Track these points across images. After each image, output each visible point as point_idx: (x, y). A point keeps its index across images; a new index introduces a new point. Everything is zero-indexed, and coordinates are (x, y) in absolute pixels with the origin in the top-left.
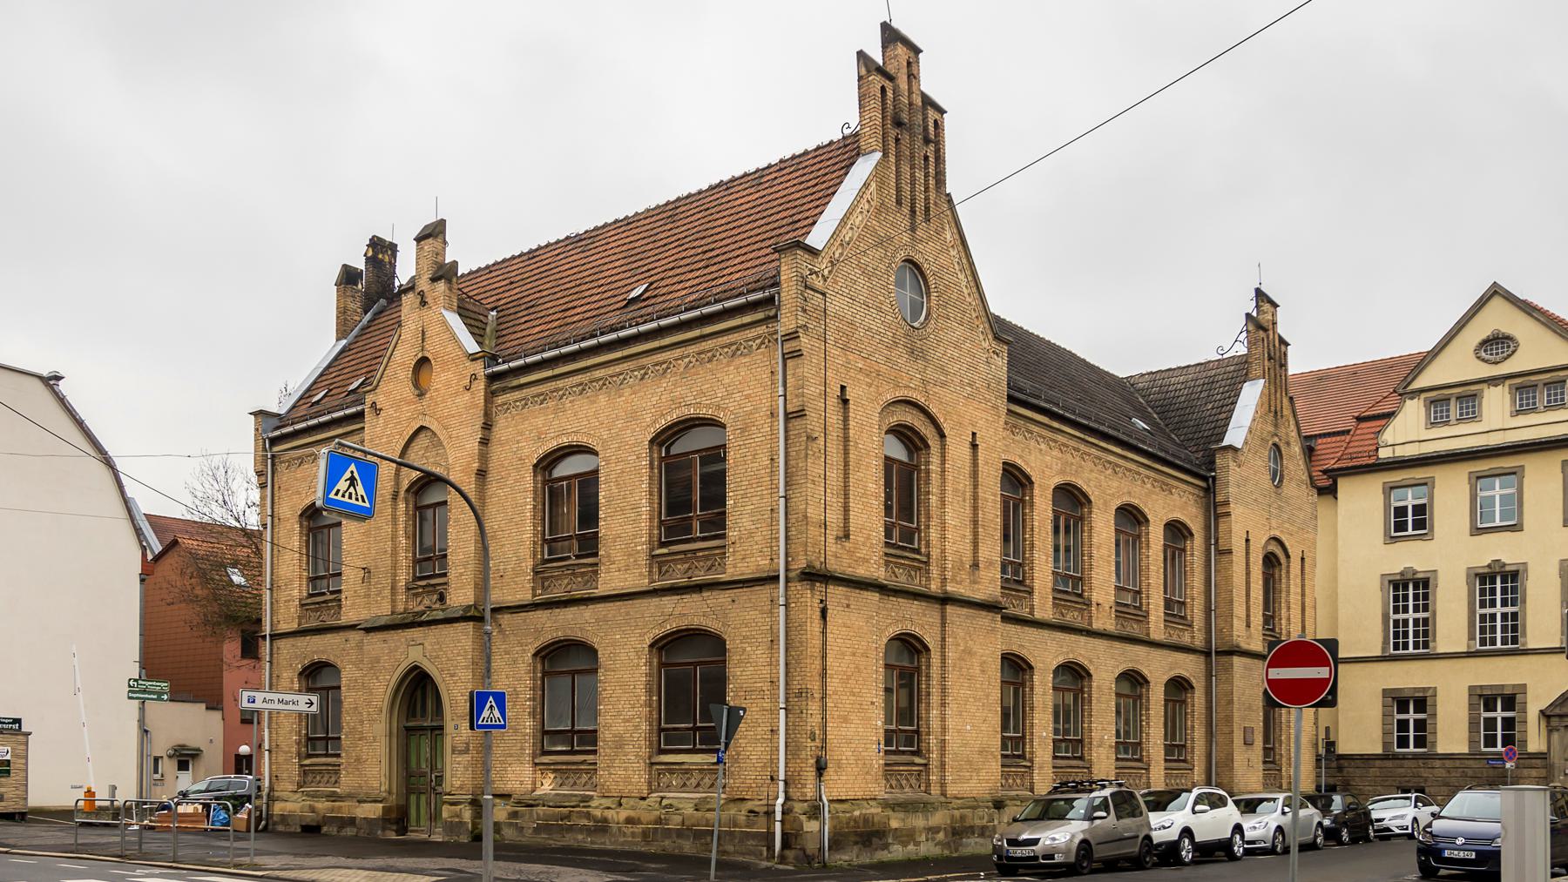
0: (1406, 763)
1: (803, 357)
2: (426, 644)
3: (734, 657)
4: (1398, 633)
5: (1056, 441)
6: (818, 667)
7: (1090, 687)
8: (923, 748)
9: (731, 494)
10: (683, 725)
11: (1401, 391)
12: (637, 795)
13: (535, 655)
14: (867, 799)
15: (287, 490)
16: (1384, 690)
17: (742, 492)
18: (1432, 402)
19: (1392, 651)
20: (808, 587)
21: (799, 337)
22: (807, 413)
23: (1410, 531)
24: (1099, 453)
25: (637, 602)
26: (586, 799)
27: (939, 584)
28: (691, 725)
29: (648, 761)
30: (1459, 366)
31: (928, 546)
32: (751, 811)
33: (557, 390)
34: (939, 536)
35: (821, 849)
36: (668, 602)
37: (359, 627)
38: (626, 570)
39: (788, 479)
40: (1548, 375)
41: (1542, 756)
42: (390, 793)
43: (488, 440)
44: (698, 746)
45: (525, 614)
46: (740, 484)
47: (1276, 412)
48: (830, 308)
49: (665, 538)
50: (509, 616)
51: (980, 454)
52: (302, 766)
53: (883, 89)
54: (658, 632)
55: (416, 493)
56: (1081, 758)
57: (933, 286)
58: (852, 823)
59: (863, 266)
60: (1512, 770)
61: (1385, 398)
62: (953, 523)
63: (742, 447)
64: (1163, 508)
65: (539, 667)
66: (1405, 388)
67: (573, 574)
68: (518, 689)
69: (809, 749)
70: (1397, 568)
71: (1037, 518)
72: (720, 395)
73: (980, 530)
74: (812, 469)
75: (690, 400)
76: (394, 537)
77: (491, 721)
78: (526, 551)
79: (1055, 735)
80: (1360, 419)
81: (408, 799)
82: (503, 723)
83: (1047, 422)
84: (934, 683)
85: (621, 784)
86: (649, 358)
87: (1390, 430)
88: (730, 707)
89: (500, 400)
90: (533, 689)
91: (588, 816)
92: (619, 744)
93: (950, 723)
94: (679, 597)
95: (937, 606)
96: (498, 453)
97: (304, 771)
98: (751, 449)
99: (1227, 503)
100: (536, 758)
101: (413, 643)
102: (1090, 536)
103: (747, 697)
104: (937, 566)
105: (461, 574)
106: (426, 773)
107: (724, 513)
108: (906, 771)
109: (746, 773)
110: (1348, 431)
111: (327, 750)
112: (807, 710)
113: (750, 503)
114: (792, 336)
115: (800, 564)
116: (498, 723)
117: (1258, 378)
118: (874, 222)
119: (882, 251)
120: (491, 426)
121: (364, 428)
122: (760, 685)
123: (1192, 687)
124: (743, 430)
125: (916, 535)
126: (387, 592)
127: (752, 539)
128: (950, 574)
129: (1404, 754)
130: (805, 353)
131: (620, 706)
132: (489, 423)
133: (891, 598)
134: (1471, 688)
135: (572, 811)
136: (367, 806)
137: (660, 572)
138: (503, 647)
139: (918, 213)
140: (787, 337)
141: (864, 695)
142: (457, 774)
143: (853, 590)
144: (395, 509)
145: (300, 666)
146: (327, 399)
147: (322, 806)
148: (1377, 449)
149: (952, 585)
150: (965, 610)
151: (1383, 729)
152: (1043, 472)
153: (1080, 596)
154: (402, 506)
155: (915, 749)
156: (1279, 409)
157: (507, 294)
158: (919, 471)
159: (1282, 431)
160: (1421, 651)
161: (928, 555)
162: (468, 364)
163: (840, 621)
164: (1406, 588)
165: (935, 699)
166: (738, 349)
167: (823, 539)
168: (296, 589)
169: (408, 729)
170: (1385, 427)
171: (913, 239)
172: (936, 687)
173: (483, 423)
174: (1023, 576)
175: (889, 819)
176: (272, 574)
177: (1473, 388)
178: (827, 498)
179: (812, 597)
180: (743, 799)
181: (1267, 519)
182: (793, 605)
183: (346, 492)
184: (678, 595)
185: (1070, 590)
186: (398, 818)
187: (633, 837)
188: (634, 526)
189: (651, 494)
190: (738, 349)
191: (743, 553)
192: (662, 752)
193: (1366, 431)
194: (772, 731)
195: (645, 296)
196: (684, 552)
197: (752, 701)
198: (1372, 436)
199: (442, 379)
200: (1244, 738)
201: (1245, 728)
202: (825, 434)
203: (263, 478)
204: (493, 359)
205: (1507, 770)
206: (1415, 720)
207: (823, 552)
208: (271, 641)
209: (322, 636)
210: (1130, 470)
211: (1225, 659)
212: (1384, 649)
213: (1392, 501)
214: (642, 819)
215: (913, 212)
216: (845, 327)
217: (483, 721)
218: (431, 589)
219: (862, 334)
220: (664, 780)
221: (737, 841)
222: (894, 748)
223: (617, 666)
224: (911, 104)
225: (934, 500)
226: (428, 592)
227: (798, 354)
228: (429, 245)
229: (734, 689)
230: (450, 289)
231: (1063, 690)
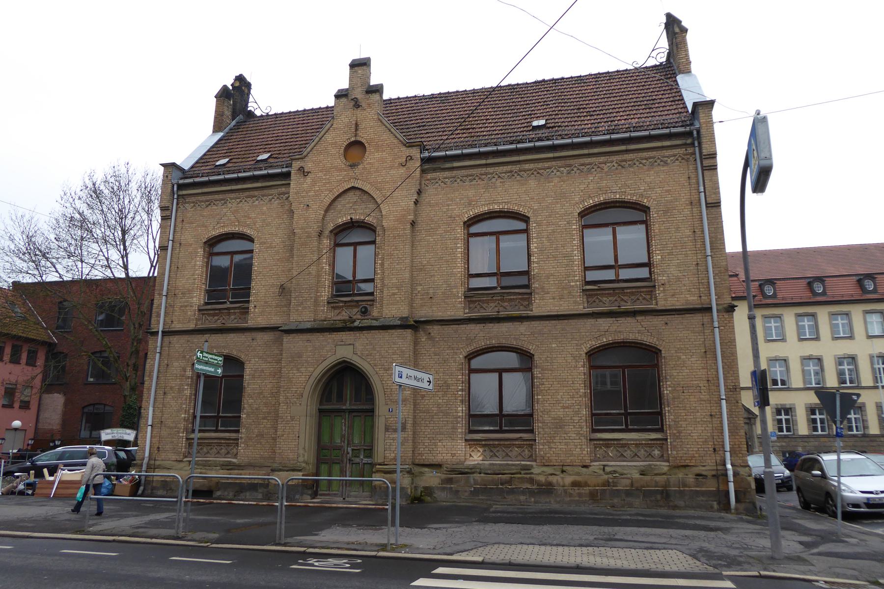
2: (357, 344)
3: (670, 363)
10: (614, 411)
12: (579, 464)
25: (573, 322)
26: (527, 468)
28: (216, 414)
33: (486, 174)
37: (280, 329)
39: (169, 287)
45: (457, 326)
46: (666, 246)
50: (440, 327)
55: (336, 235)
63: (665, 222)
67: (501, 300)
75: (615, 189)
85: (562, 455)
91: (531, 481)
92: (559, 424)
94: (614, 319)
98: (674, 224)
103: (685, 391)
105: (394, 294)
109: (689, 446)
111: (217, 426)
113: (676, 259)
122: (696, 382)
124: (666, 212)
127: (680, 283)
131: (559, 397)
135: (514, 477)
138: (433, 349)
140: (708, 157)
147: (215, 474)
162: (403, 149)
187: (580, 497)
188: (567, 268)
191: (673, 291)
194: (711, 415)
197: (690, 394)
203: (167, 213)
208: (163, 336)
209: (224, 335)
214: (589, 482)
218: (355, 304)
226: (348, 306)
229: (672, 385)
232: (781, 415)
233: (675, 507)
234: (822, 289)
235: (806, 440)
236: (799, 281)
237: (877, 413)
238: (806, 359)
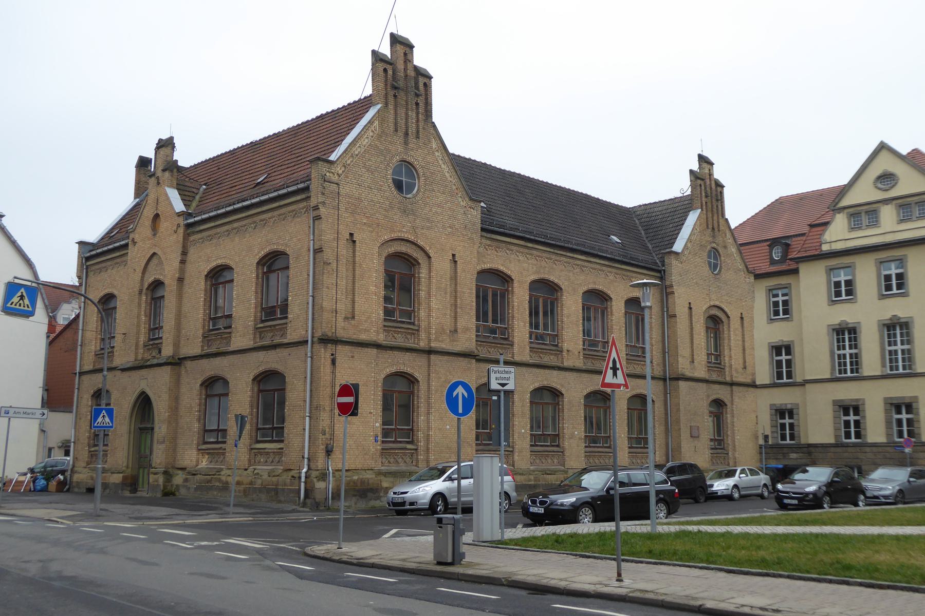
0: (850, 449)
1: (322, 219)
5: (532, 255)
6: (329, 392)
7: (563, 401)
8: (415, 440)
9: (290, 294)
11: (832, 208)
13: (201, 385)
14: (365, 470)
15: (92, 287)
17: (295, 293)
18: (851, 215)
20: (322, 346)
21: (319, 208)
22: (324, 250)
23: (844, 297)
24: (569, 260)
27: (427, 342)
29: (249, 447)
30: (864, 193)
31: (419, 320)
32: (293, 477)
34: (427, 314)
35: (326, 499)
36: (261, 355)
38: (244, 336)
42: (127, 467)
43: (185, 261)
44: (274, 438)
47: (713, 229)
48: (342, 192)
49: (265, 318)
51: (458, 266)
52: (90, 451)
53: (385, 70)
54: (257, 372)
56: (558, 446)
57: (422, 174)
58: (352, 484)
59: (368, 167)
60: (910, 454)
61: (823, 215)
62: (436, 307)
64: (624, 290)
65: (204, 392)
66: (834, 206)
67: (221, 338)
68: (193, 405)
69: (321, 440)
70: (887, 316)
71: (516, 300)
72: (287, 239)
73: (458, 310)
74: (327, 280)
76: (139, 316)
77: (103, 424)
78: (199, 324)
79: (531, 431)
81: (138, 472)
82: (111, 425)
83: (523, 244)
84: (422, 400)
86: (257, 217)
88: (242, 416)
89: (192, 238)
90: (200, 405)
91: (220, 480)
93: (433, 425)
94: (266, 352)
95: (425, 355)
96: (190, 268)
97: (91, 455)
99: (671, 286)
100: (199, 446)
101: (142, 378)
102: (562, 310)
103: (294, 410)
104: (425, 332)
106: (148, 455)
107: (287, 304)
108: (402, 453)
112: (320, 417)
114: (316, 208)
115: (318, 334)
116: (108, 425)
118: (376, 142)
119: (382, 157)
120: (187, 253)
121: (128, 253)
124: (297, 258)
125: (413, 314)
126: (133, 348)
128: (434, 336)
130: (323, 217)
132: (186, 251)
133: (388, 351)
134: (886, 399)
136: (115, 475)
137: (260, 337)
139: (410, 135)
141: (364, 408)
142: (159, 457)
143: (356, 348)
144: (140, 299)
145: (92, 391)
146: (118, 234)
148: (821, 245)
149: (435, 343)
150: (446, 357)
151: (834, 427)
152: (521, 273)
153: (557, 346)
154: (144, 298)
155: (411, 440)
156: (716, 226)
157: (214, 176)
158: (415, 277)
159: (719, 239)
160: (855, 374)
161: (419, 326)
163: (346, 365)
165: (422, 409)
166: (296, 214)
167: (335, 319)
168: (93, 346)
169: (141, 429)
170: (824, 231)
171: (406, 149)
172: (424, 403)
173: (182, 252)
174: (508, 336)
175: (381, 482)
176: (82, 337)
178: (338, 296)
179: (325, 352)
180: (291, 470)
181: (707, 294)
182: (315, 357)
183: (17, 303)
184: (265, 350)
185: (548, 343)
186: (132, 484)
189: (256, 293)
190: (296, 214)
192: (258, 442)
193: (815, 233)
195: (263, 182)
196: (270, 326)
199: (165, 226)
200: (691, 433)
201: (691, 426)
202: (337, 260)
203: (81, 280)
204: (190, 215)
207: (334, 326)
210: (595, 269)
211: (674, 383)
212: (832, 373)
213: (832, 278)
215: (406, 134)
216: (353, 201)
217: (97, 424)
219: (366, 204)
220: (258, 458)
221: (285, 494)
222: (393, 439)
223: (238, 391)
224: (406, 76)
225: (423, 294)
227: (318, 217)
228: (163, 151)
230: (172, 176)
231: (537, 403)
233: (280, 502)
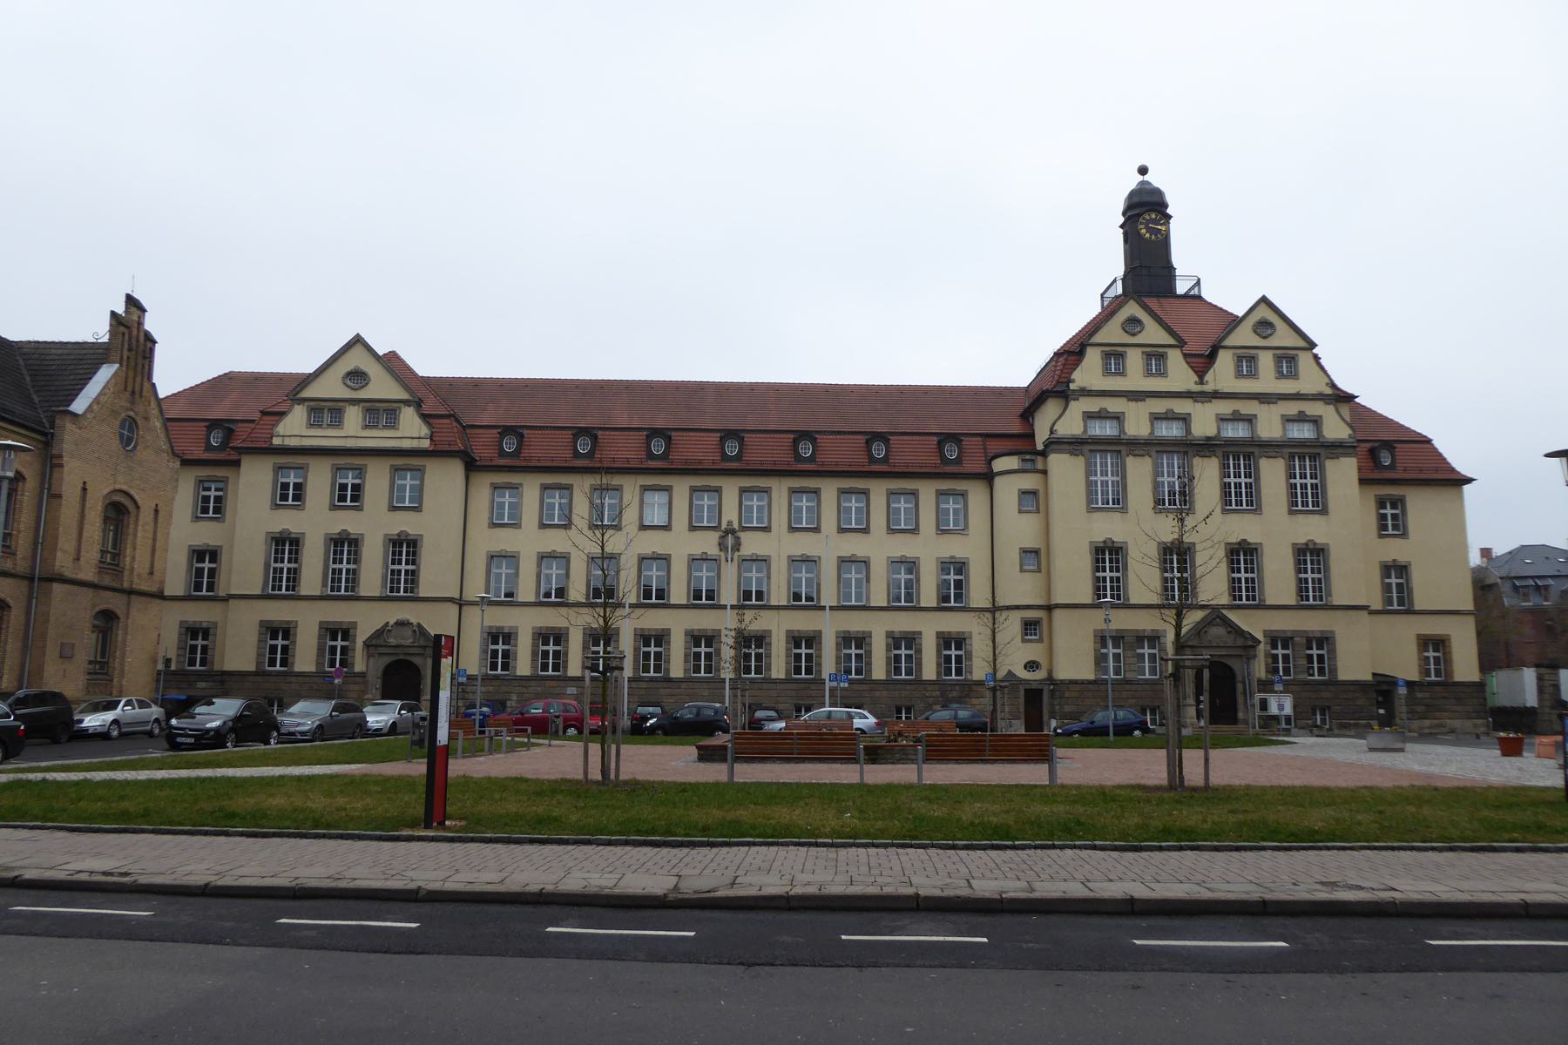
4: (1099, 590)
16: (261, 621)
18: (367, 410)
19: (329, 592)
30: (330, 388)
40: (386, 404)
41: (362, 675)
60: (339, 685)
70: (394, 531)
80: (264, 413)
87: (281, 425)
99: (60, 456)
110: (254, 421)
117: (114, 362)
123: (9, 607)
129: (495, 675)
160: (291, 592)
164: (1104, 554)
170: (278, 422)
177: (340, 404)
198: (270, 427)
201: (62, 643)
205: (336, 684)
206: (705, 653)
212: (263, 590)
232: (1277, 649)
234: (1390, 460)
235: (524, 683)
236: (631, 433)
237: (635, 645)
238: (844, 562)
